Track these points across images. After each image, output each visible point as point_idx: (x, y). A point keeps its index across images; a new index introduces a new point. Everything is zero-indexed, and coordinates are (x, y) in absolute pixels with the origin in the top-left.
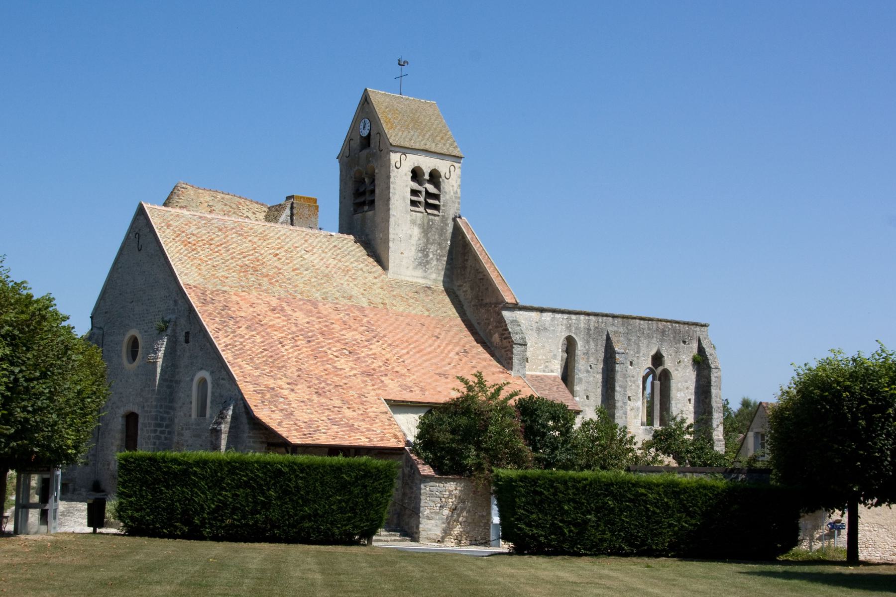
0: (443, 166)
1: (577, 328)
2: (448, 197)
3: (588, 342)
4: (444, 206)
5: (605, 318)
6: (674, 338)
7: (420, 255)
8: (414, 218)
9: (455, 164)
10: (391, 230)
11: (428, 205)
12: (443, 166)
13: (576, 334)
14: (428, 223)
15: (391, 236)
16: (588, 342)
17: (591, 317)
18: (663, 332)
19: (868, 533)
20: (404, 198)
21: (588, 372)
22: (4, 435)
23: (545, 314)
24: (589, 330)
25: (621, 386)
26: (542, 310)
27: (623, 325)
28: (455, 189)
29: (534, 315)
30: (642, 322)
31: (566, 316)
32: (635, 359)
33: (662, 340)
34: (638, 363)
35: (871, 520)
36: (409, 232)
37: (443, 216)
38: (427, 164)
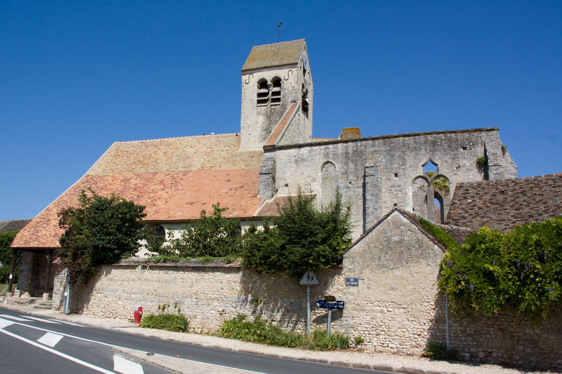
0: (282, 73)
1: (334, 155)
2: (286, 91)
3: (346, 163)
4: (283, 97)
5: (364, 142)
6: (449, 146)
7: (264, 132)
8: (260, 110)
9: (292, 69)
10: (242, 122)
11: (273, 100)
12: (282, 73)
13: (334, 159)
14: (271, 110)
15: (242, 125)
16: (346, 163)
17: (349, 143)
18: (434, 143)
19: (379, 315)
20: (252, 100)
21: (348, 188)
22: (561, 359)
23: (303, 149)
24: (347, 154)
25: (372, 195)
26: (300, 146)
27: (385, 144)
28: (293, 84)
29: (293, 151)
30: (406, 138)
31: (323, 147)
32: (401, 171)
33: (433, 151)
34: (405, 174)
35: (383, 297)
36: (256, 120)
37: (283, 104)
38: (269, 75)
